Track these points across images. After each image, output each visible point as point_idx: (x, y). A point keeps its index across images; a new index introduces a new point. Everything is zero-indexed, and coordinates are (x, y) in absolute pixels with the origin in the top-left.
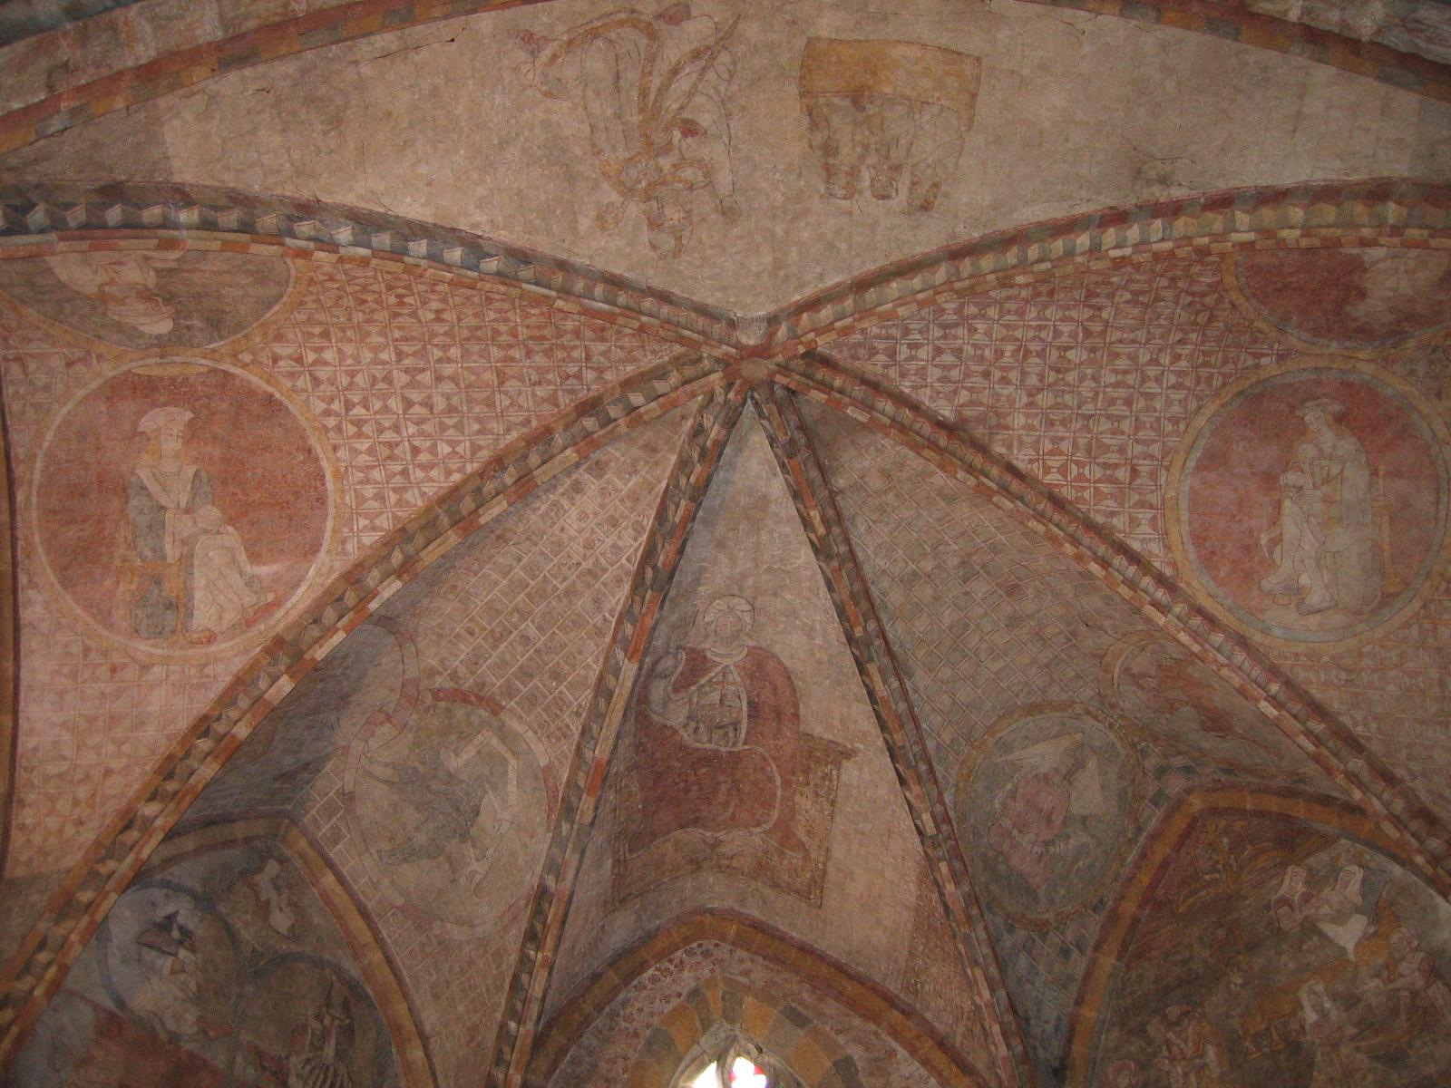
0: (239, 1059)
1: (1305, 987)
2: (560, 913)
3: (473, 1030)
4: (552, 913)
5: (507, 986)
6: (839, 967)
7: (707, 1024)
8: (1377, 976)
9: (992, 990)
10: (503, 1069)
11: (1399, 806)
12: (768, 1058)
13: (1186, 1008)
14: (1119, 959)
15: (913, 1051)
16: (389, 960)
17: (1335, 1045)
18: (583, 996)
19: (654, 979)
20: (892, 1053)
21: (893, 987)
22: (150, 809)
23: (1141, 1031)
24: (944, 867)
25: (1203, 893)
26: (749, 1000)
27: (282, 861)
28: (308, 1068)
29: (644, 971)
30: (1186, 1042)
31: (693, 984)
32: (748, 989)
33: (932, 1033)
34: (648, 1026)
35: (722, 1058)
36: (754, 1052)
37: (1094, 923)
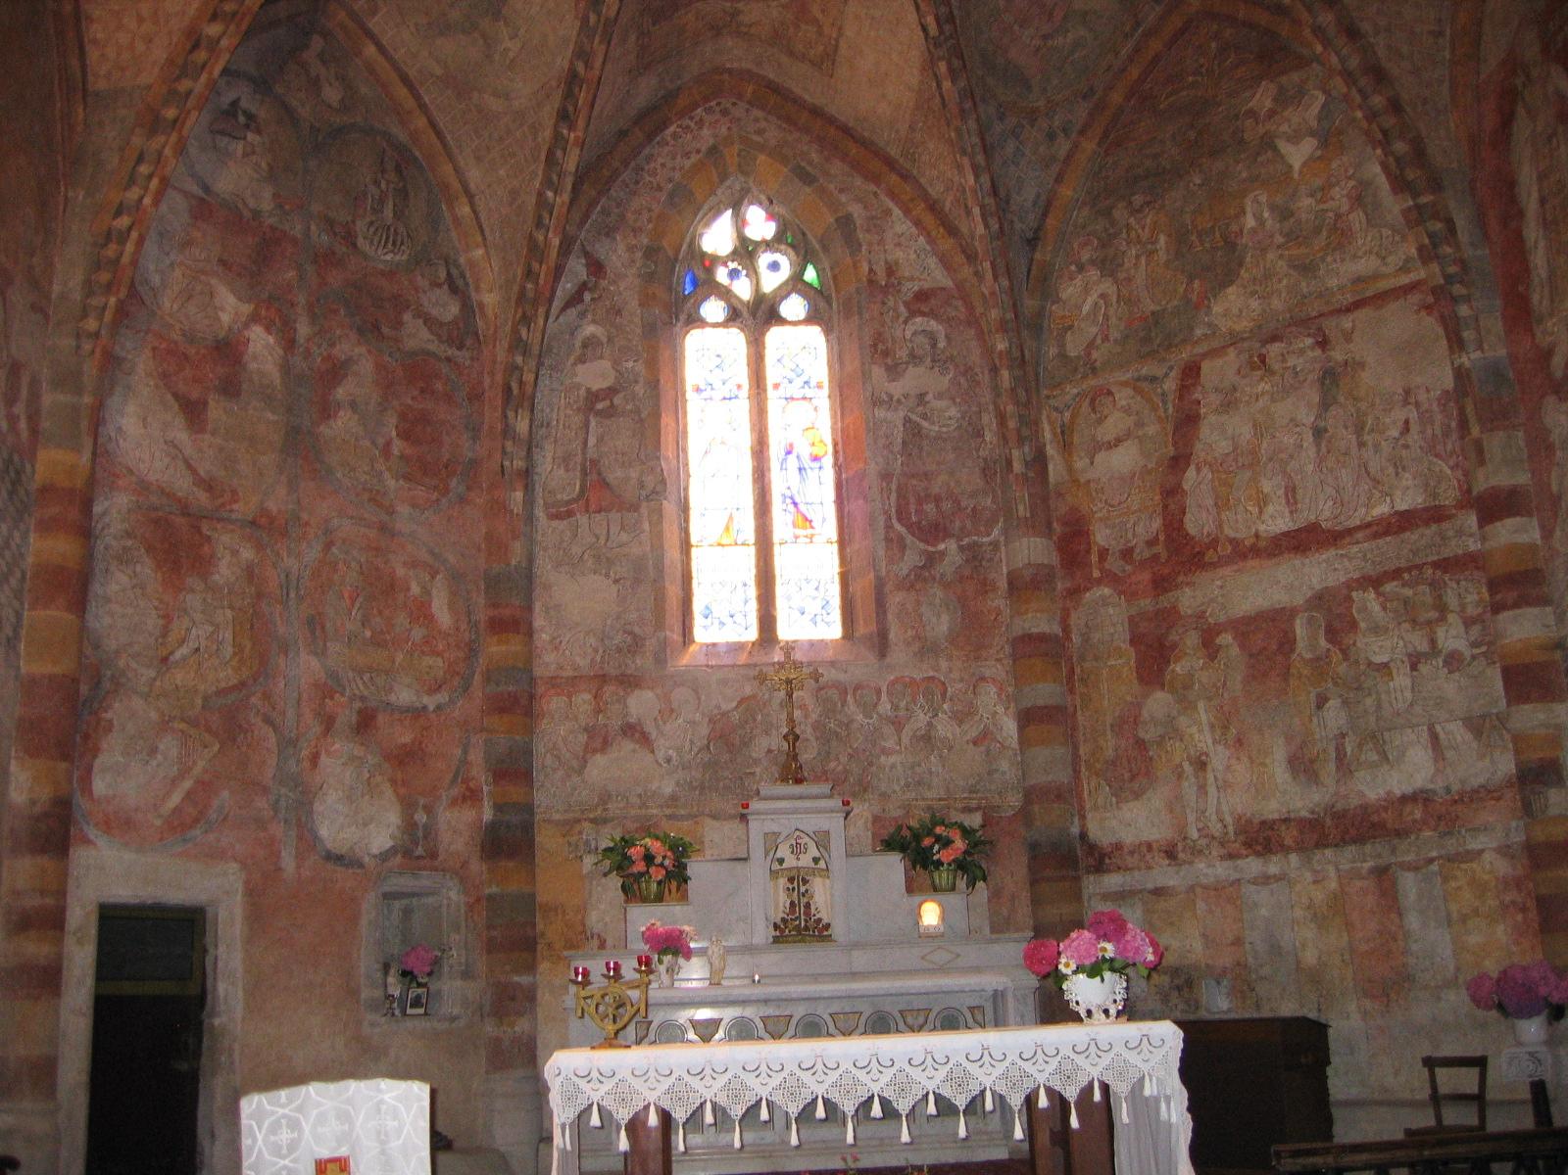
0: (313, 227)
1: (1252, 195)
2: (590, 97)
3: (514, 194)
4: (583, 97)
5: (543, 157)
6: (845, 130)
7: (723, 177)
8: (1312, 196)
9: (977, 177)
10: (543, 231)
11: (1354, 63)
12: (778, 209)
13: (1148, 199)
14: (1099, 145)
15: (907, 212)
16: (433, 125)
17: (1264, 251)
18: (610, 152)
19: (675, 136)
20: (888, 212)
21: (894, 151)
22: (213, 30)
23: (1107, 213)
24: (942, 67)
25: (1184, 93)
26: (762, 158)
27: (326, 35)
28: (372, 230)
29: (667, 128)
30: (1143, 228)
31: (711, 141)
32: (762, 148)
33: (925, 197)
34: (670, 180)
35: (737, 207)
36: (766, 202)
37: (1082, 111)
